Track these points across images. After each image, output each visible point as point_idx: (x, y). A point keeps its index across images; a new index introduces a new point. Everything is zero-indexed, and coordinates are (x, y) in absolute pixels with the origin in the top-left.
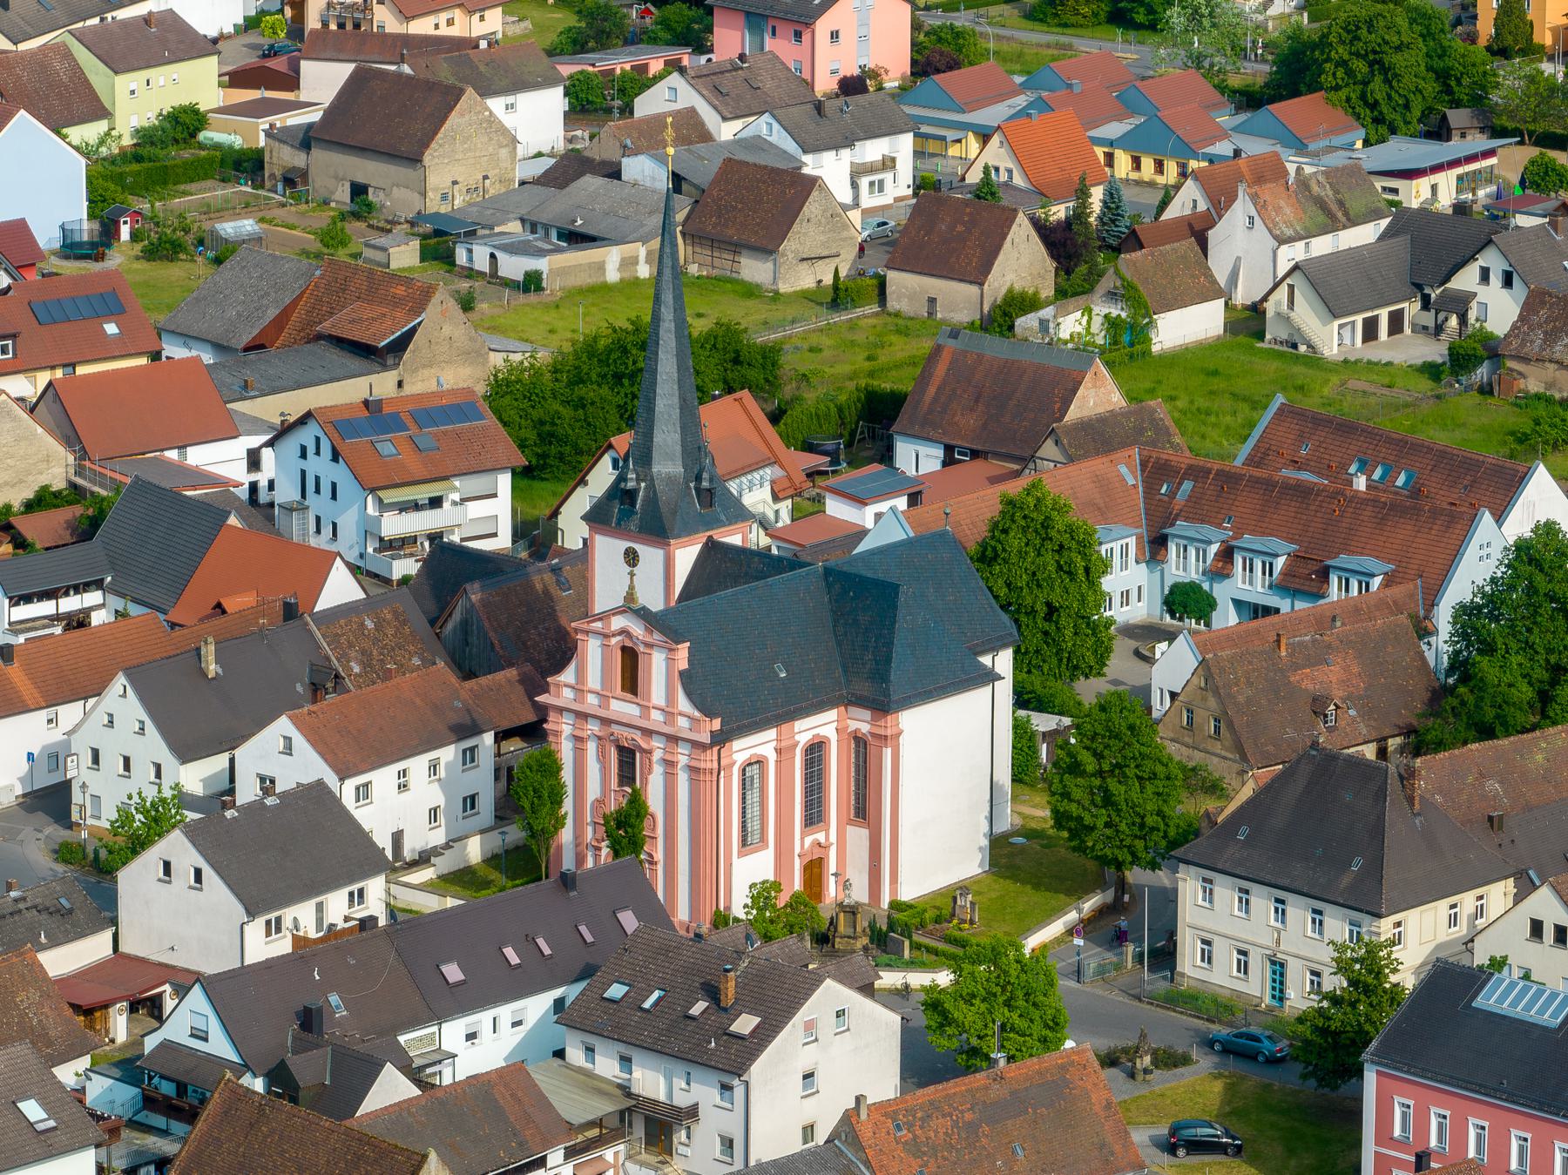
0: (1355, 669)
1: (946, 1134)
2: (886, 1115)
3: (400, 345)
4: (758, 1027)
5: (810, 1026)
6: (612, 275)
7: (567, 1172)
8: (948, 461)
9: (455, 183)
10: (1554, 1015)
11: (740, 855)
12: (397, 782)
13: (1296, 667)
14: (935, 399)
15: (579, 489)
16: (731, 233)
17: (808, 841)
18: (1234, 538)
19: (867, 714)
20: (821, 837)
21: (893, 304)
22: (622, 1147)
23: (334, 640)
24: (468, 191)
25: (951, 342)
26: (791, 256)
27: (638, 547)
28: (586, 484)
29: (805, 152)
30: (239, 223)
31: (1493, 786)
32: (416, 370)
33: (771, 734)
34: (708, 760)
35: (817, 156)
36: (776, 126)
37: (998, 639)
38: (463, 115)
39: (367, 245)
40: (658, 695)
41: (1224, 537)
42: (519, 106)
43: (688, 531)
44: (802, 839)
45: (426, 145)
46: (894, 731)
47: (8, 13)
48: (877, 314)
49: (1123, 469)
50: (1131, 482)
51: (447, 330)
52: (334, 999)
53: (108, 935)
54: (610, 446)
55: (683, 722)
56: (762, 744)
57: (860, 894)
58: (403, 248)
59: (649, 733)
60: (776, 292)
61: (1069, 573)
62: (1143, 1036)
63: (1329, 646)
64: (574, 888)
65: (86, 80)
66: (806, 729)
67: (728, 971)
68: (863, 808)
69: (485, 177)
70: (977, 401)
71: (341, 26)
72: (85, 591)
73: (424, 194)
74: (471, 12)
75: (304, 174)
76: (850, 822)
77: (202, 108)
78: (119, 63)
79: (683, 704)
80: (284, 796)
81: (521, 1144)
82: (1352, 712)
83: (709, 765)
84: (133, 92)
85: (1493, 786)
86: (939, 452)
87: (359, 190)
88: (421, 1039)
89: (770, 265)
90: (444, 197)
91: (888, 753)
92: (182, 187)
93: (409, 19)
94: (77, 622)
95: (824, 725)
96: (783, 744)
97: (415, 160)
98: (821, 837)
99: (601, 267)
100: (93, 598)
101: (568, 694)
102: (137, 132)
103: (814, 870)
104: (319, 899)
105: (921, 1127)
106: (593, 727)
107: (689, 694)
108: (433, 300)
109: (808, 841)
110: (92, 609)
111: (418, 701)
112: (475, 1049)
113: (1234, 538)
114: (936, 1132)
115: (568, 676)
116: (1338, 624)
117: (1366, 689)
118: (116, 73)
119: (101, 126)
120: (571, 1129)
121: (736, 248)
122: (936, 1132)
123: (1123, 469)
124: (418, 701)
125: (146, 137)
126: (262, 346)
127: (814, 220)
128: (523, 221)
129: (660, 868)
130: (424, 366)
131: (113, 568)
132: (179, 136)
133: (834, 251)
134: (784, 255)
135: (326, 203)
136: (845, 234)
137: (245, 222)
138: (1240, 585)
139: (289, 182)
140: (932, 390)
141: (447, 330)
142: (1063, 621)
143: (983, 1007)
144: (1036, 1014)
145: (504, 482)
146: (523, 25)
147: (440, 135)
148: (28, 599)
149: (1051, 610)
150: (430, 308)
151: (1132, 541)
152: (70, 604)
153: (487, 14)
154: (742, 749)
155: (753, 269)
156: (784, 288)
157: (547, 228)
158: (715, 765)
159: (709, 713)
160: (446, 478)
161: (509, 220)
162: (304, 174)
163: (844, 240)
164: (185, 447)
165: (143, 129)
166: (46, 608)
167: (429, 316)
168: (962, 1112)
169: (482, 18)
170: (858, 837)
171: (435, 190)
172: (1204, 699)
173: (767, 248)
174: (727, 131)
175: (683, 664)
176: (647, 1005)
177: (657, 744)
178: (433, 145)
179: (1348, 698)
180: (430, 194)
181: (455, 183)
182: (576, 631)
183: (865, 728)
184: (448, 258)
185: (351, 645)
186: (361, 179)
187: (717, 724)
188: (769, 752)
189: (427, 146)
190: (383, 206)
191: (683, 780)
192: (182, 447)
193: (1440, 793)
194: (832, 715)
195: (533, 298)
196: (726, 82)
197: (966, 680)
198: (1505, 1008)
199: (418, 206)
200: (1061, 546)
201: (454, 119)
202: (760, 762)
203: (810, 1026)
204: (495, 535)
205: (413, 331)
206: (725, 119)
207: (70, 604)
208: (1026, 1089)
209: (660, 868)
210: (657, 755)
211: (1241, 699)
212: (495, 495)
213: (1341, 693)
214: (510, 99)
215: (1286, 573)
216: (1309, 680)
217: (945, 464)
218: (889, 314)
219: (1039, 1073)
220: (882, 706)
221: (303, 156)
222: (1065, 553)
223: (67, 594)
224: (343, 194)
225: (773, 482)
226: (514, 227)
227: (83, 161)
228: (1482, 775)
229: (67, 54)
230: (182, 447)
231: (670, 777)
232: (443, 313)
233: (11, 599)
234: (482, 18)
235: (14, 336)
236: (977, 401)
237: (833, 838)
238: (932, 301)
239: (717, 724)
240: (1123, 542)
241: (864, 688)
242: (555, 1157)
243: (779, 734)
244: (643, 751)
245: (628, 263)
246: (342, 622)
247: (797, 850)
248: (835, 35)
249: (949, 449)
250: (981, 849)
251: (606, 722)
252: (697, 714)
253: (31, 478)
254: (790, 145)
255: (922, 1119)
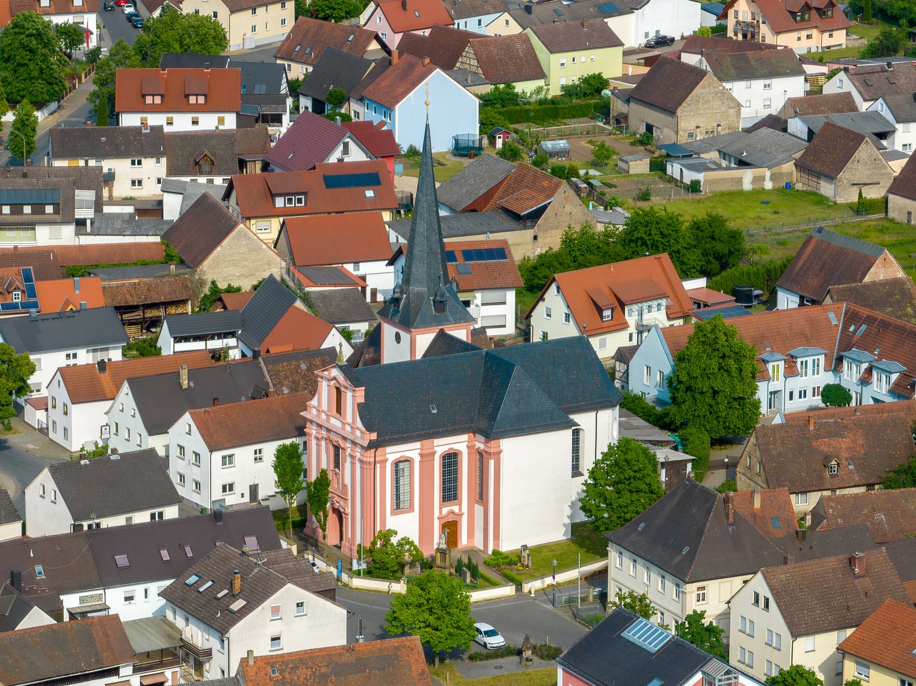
0: (861, 442)
1: (305, 678)
2: (268, 664)
3: (536, 215)
4: (243, 607)
5: (275, 610)
6: (747, 186)
7: (135, 680)
8: (801, 304)
9: (698, 127)
10: (655, 646)
11: (392, 514)
12: (253, 456)
13: (818, 437)
14: (801, 268)
15: (541, 303)
16: (817, 167)
17: (445, 510)
18: (877, 360)
19: (482, 439)
20: (456, 509)
21: (891, 214)
22: (178, 669)
23: (275, 374)
24: (707, 132)
25: (817, 235)
26: (845, 181)
27: (401, 333)
28: (544, 300)
29: (898, 122)
30: (557, 142)
31: (881, 517)
32: (547, 230)
33: (418, 445)
34: (369, 456)
35: (906, 125)
36: (885, 105)
37: (599, 403)
38: (704, 88)
39: (620, 160)
40: (349, 419)
41: (871, 359)
42: (773, 86)
43: (426, 324)
44: (441, 509)
45: (679, 104)
46: (496, 450)
47: (530, 16)
48: (881, 219)
49: (832, 315)
50: (834, 322)
51: (568, 208)
52: (39, 568)
53: (18, 525)
54: (554, 280)
55: (358, 433)
56: (412, 450)
57: (479, 545)
58: (638, 162)
59: (345, 439)
60: (835, 203)
61: (727, 371)
62: (527, 639)
63: (846, 426)
64: (220, 520)
65: (536, 56)
66: (442, 445)
67: (236, 573)
68: (481, 496)
69: (719, 125)
70: (821, 271)
71: (745, 36)
72: (225, 337)
73: (677, 133)
74: (823, 32)
75: (626, 117)
76: (477, 502)
77: (605, 76)
78: (554, 47)
79: (359, 424)
80: (121, 455)
81: (97, 661)
82: (851, 467)
83: (368, 460)
84: (563, 64)
85: (881, 517)
86: (797, 300)
87: (649, 128)
88: (92, 597)
89: (833, 186)
90: (691, 135)
91: (492, 463)
92: (566, 121)
93: (778, 33)
94: (217, 355)
95: (460, 443)
96: (424, 452)
97: (672, 113)
98: (456, 509)
99: (740, 181)
100: (232, 342)
101: (314, 412)
102: (563, 88)
103: (451, 528)
104: (128, 515)
105: (289, 673)
106: (324, 433)
107: (361, 418)
108: (559, 190)
109: (445, 510)
110: (230, 348)
111: (281, 411)
112: (130, 606)
113: (877, 360)
114: (299, 677)
115: (314, 402)
116: (858, 414)
117: (865, 454)
118: (551, 53)
119: (541, 83)
120: (135, 655)
121: (819, 175)
122: (299, 677)
123: (832, 315)
124: (281, 411)
125: (569, 91)
126: (474, 211)
127: (861, 162)
128: (719, 152)
129: (349, 517)
130: (552, 228)
131: (243, 326)
132: (588, 92)
133: (876, 181)
134: (840, 181)
135: (635, 134)
136: (884, 171)
137: (561, 141)
138: (875, 389)
139: (618, 121)
140: (801, 262)
141: (568, 208)
142: (719, 399)
143: (415, 611)
144: (447, 618)
145: (511, 296)
146: (860, 41)
147: (688, 99)
148: (186, 339)
149: (715, 393)
150: (557, 194)
151: (822, 358)
152: (215, 344)
153: (834, 33)
154: (393, 453)
155: (826, 189)
156: (839, 201)
157: (730, 156)
158: (373, 460)
159: (369, 429)
160: (472, 291)
161: (711, 151)
162: (626, 117)
163: (884, 174)
164: (358, 262)
165: (567, 86)
166: (199, 345)
167: (557, 200)
168: (320, 667)
169: (831, 36)
170: (479, 509)
171: (684, 130)
172: (755, 451)
173: (831, 177)
174: (864, 106)
175: (362, 400)
176: (201, 590)
177: (348, 445)
178: (684, 104)
179: (851, 458)
180: (681, 133)
181: (698, 127)
182: (318, 376)
183: (482, 447)
184: (664, 170)
185: (286, 377)
186: (650, 122)
187: (374, 436)
188: (415, 456)
189: (680, 105)
190: (659, 138)
191: (358, 465)
192: (356, 263)
193: (842, 517)
194: (465, 437)
195: (691, 196)
196: (873, 80)
197: (552, 425)
198: (639, 642)
199: (673, 140)
200: (724, 355)
201: (698, 90)
202: (408, 460)
203: (275, 610)
204: (504, 326)
205: (545, 207)
206: (865, 100)
207: (215, 344)
208: (368, 658)
209: (349, 517)
210: (349, 451)
211: (774, 453)
212: (504, 303)
213: (846, 455)
214: (767, 82)
215: (897, 384)
216: (824, 446)
217: (799, 306)
218: (888, 219)
219: (380, 650)
220: (491, 433)
221: (626, 106)
222: (727, 359)
223: (213, 338)
224: (642, 130)
225: (667, 308)
226: (713, 155)
227: (477, 101)
228: (874, 510)
229: (527, 40)
230: (356, 263)
231: (353, 464)
232: (566, 199)
233: (175, 338)
234: (831, 36)
235: (305, 194)
236: (821, 271)
237: (465, 509)
238: (909, 213)
239: (374, 436)
240: (816, 358)
241: (483, 423)
242: (126, 671)
243: (422, 445)
244: (343, 449)
245: (759, 179)
246: (285, 364)
247: (436, 514)
248: (283, 22)
249: (802, 298)
250: (565, 525)
251: (329, 430)
252: (364, 429)
253: (258, 273)
254: (890, 117)
255: (292, 669)
